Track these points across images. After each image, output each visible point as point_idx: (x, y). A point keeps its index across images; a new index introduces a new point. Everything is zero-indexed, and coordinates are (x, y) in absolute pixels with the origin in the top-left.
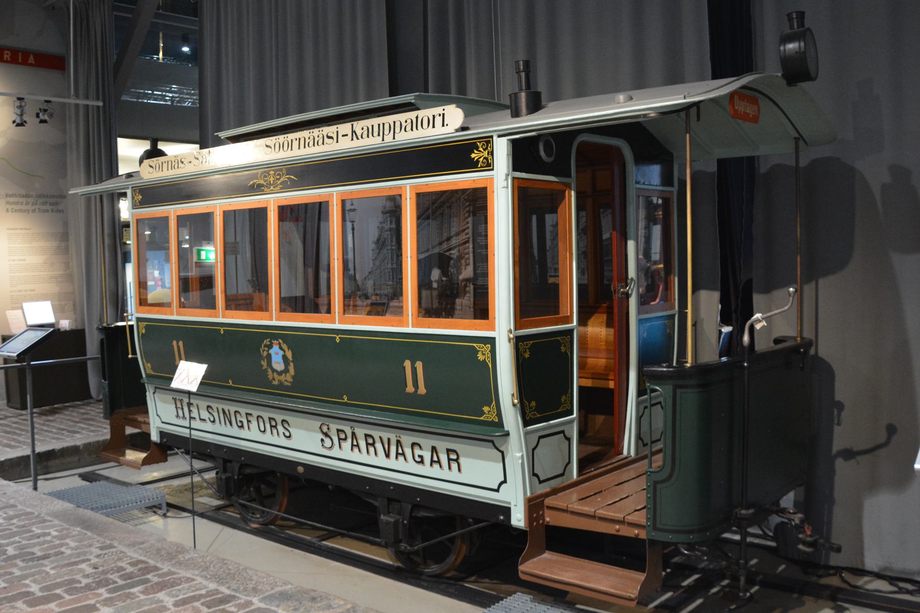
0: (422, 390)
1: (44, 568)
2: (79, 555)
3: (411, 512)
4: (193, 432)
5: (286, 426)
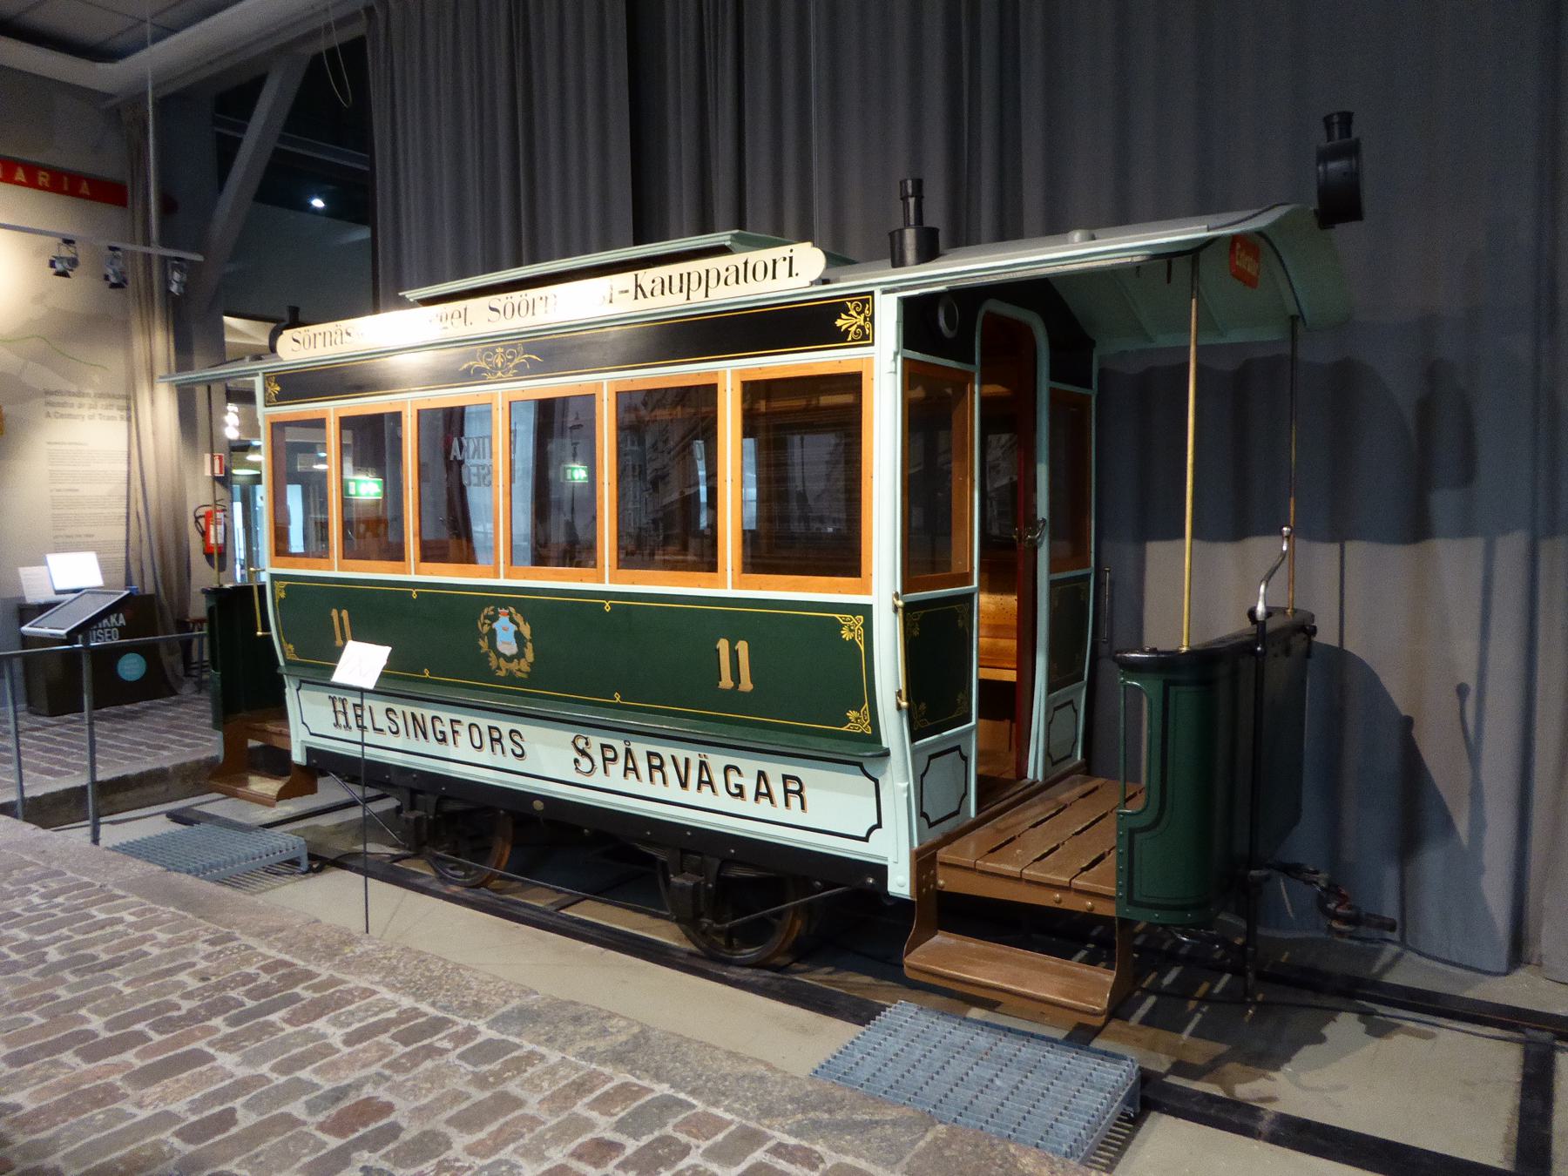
0: (746, 685)
1: (113, 984)
2: (173, 957)
3: (720, 869)
5: (517, 738)
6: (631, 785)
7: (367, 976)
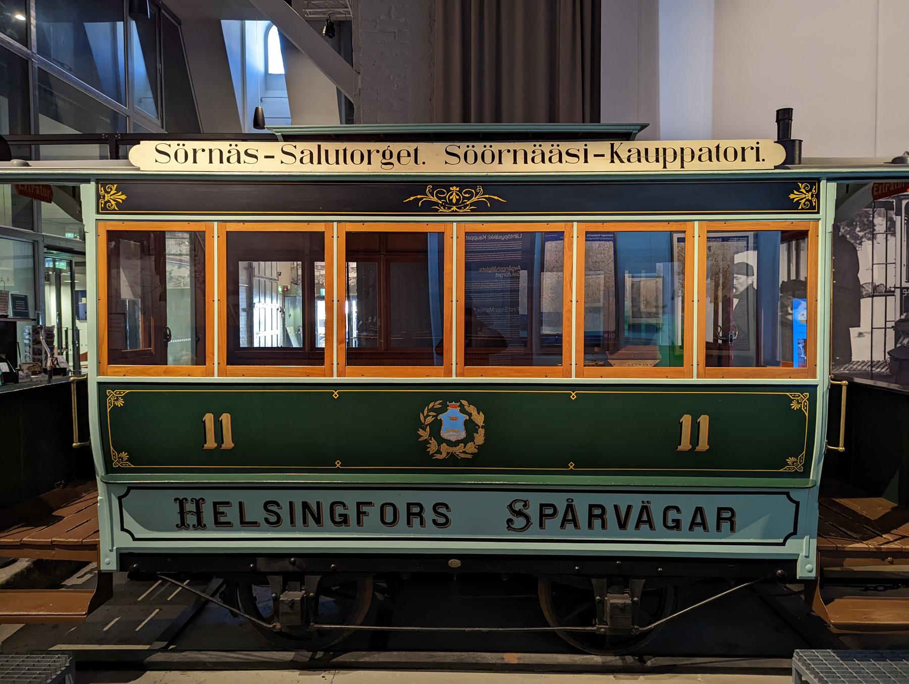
0: (228, 443)
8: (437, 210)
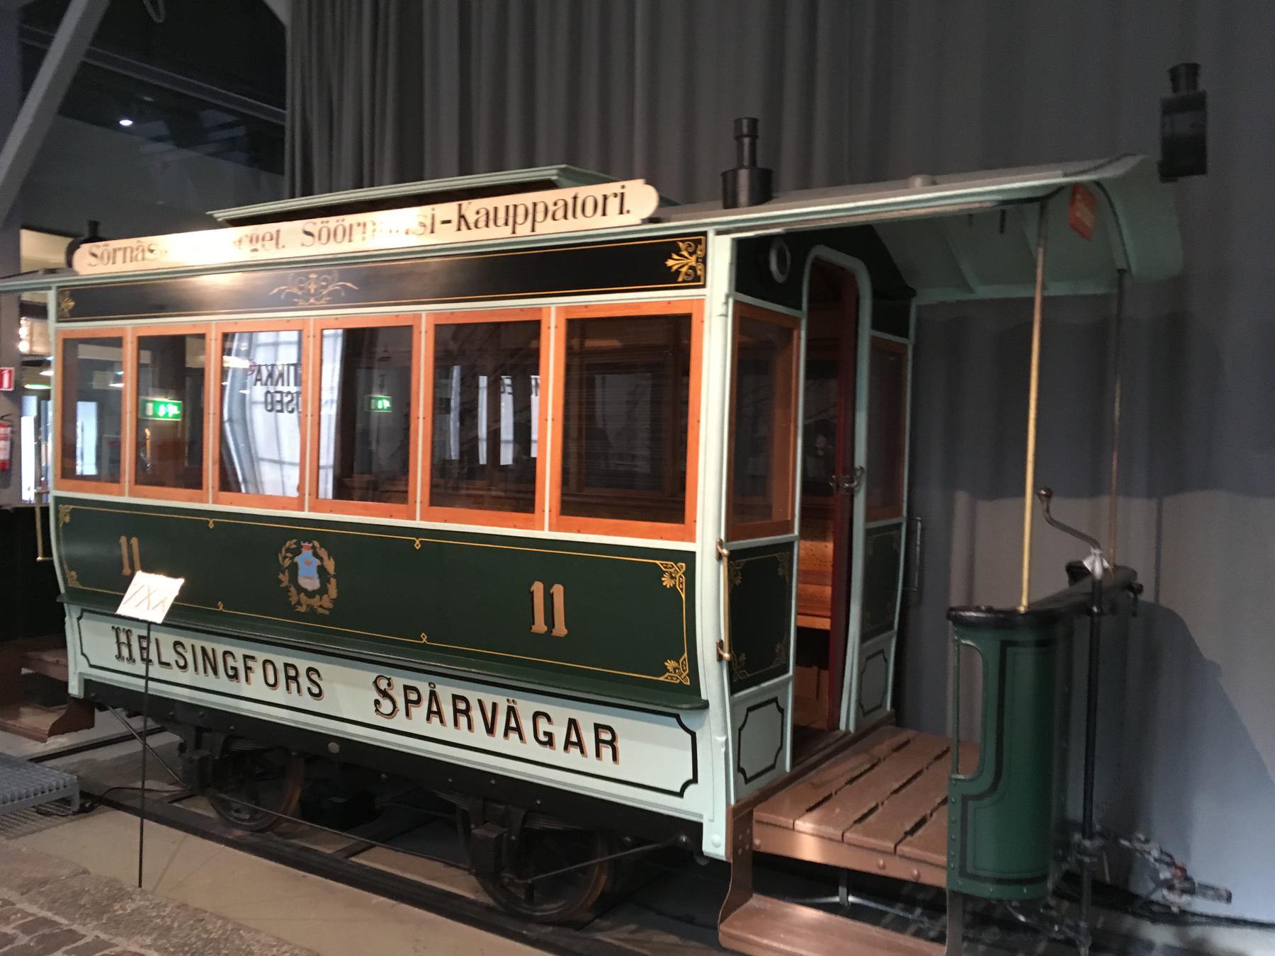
0: (561, 629)
3: (525, 820)
4: (151, 684)
5: (314, 677)
6: (434, 728)
7: (138, 937)
8: (296, 304)
